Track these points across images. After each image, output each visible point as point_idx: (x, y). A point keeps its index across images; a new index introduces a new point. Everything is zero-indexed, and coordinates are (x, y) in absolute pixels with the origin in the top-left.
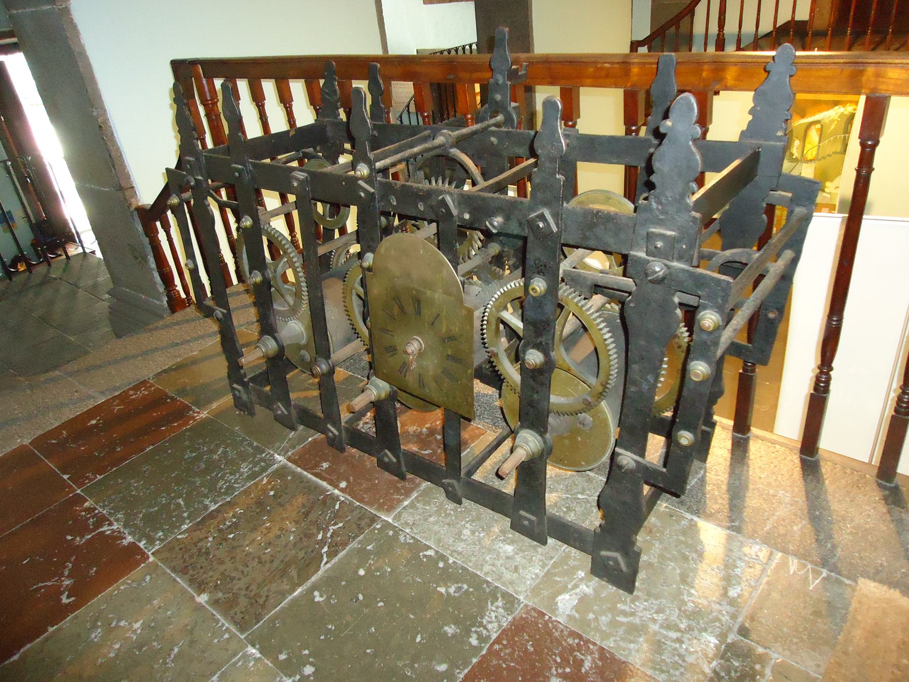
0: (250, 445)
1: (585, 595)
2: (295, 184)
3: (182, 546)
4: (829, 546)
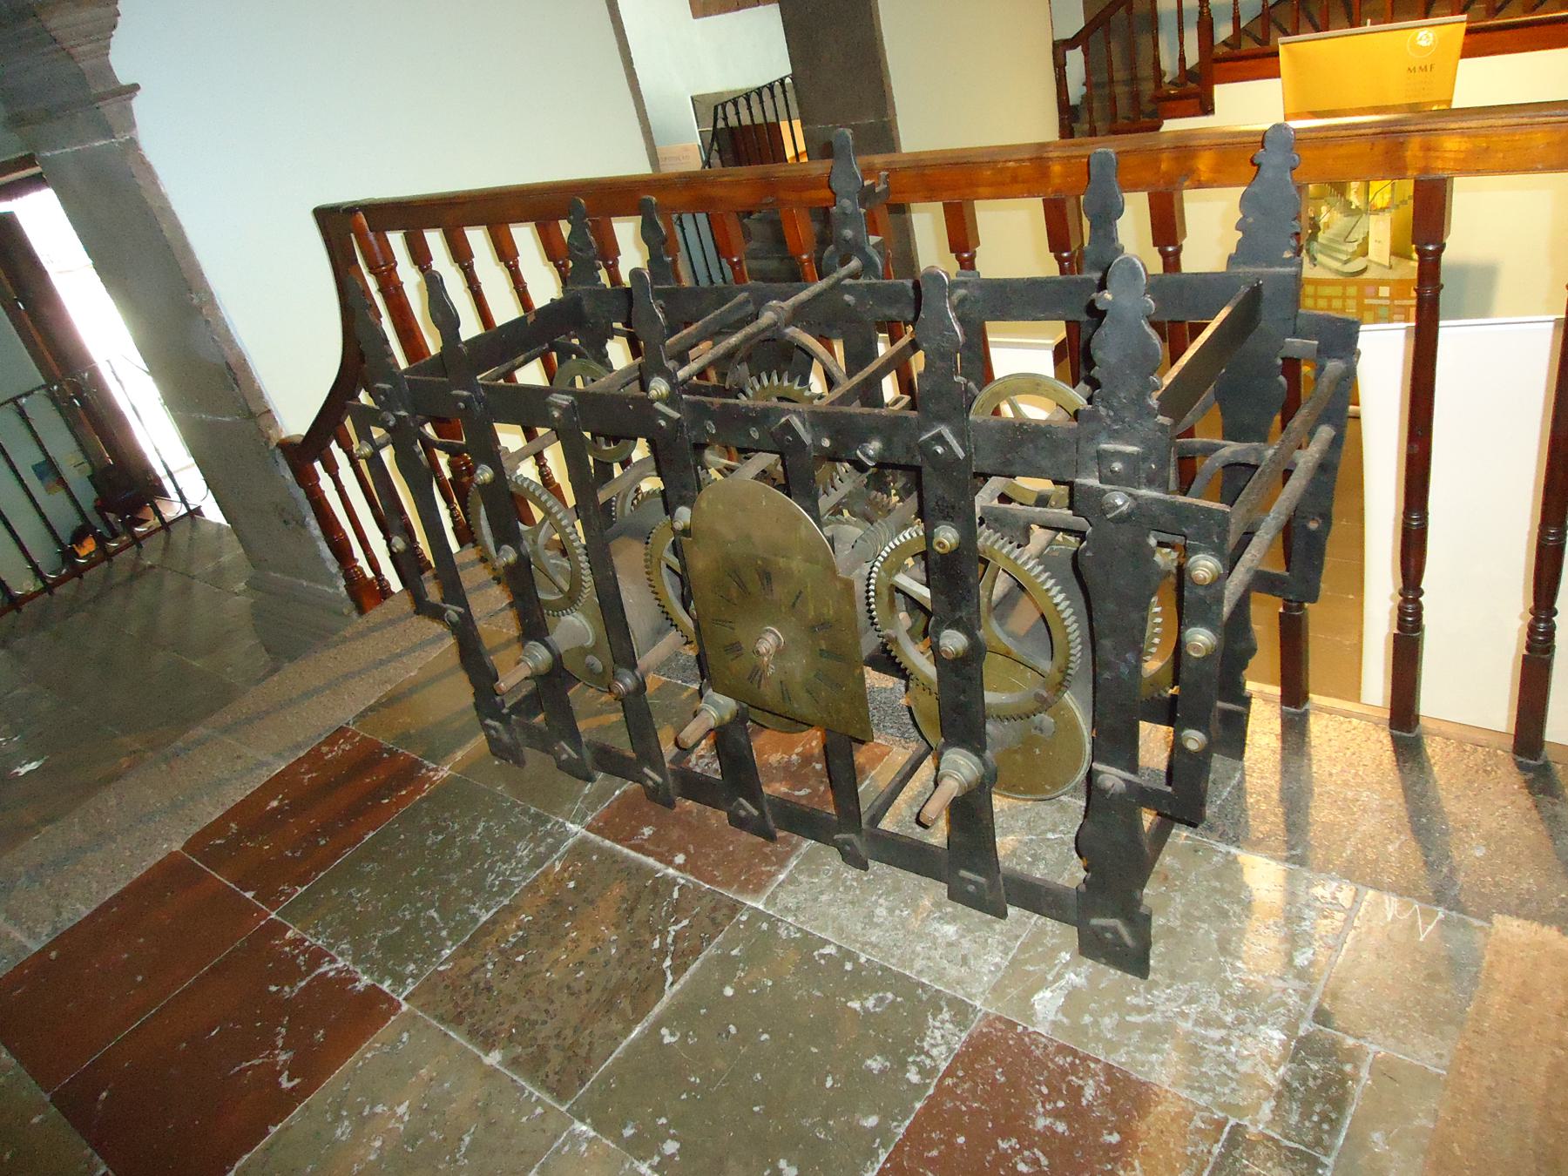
0: (525, 812)
1: (1075, 987)
2: (556, 414)
3: (448, 982)
4: (1445, 870)
